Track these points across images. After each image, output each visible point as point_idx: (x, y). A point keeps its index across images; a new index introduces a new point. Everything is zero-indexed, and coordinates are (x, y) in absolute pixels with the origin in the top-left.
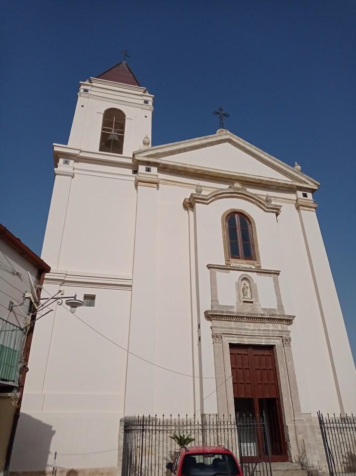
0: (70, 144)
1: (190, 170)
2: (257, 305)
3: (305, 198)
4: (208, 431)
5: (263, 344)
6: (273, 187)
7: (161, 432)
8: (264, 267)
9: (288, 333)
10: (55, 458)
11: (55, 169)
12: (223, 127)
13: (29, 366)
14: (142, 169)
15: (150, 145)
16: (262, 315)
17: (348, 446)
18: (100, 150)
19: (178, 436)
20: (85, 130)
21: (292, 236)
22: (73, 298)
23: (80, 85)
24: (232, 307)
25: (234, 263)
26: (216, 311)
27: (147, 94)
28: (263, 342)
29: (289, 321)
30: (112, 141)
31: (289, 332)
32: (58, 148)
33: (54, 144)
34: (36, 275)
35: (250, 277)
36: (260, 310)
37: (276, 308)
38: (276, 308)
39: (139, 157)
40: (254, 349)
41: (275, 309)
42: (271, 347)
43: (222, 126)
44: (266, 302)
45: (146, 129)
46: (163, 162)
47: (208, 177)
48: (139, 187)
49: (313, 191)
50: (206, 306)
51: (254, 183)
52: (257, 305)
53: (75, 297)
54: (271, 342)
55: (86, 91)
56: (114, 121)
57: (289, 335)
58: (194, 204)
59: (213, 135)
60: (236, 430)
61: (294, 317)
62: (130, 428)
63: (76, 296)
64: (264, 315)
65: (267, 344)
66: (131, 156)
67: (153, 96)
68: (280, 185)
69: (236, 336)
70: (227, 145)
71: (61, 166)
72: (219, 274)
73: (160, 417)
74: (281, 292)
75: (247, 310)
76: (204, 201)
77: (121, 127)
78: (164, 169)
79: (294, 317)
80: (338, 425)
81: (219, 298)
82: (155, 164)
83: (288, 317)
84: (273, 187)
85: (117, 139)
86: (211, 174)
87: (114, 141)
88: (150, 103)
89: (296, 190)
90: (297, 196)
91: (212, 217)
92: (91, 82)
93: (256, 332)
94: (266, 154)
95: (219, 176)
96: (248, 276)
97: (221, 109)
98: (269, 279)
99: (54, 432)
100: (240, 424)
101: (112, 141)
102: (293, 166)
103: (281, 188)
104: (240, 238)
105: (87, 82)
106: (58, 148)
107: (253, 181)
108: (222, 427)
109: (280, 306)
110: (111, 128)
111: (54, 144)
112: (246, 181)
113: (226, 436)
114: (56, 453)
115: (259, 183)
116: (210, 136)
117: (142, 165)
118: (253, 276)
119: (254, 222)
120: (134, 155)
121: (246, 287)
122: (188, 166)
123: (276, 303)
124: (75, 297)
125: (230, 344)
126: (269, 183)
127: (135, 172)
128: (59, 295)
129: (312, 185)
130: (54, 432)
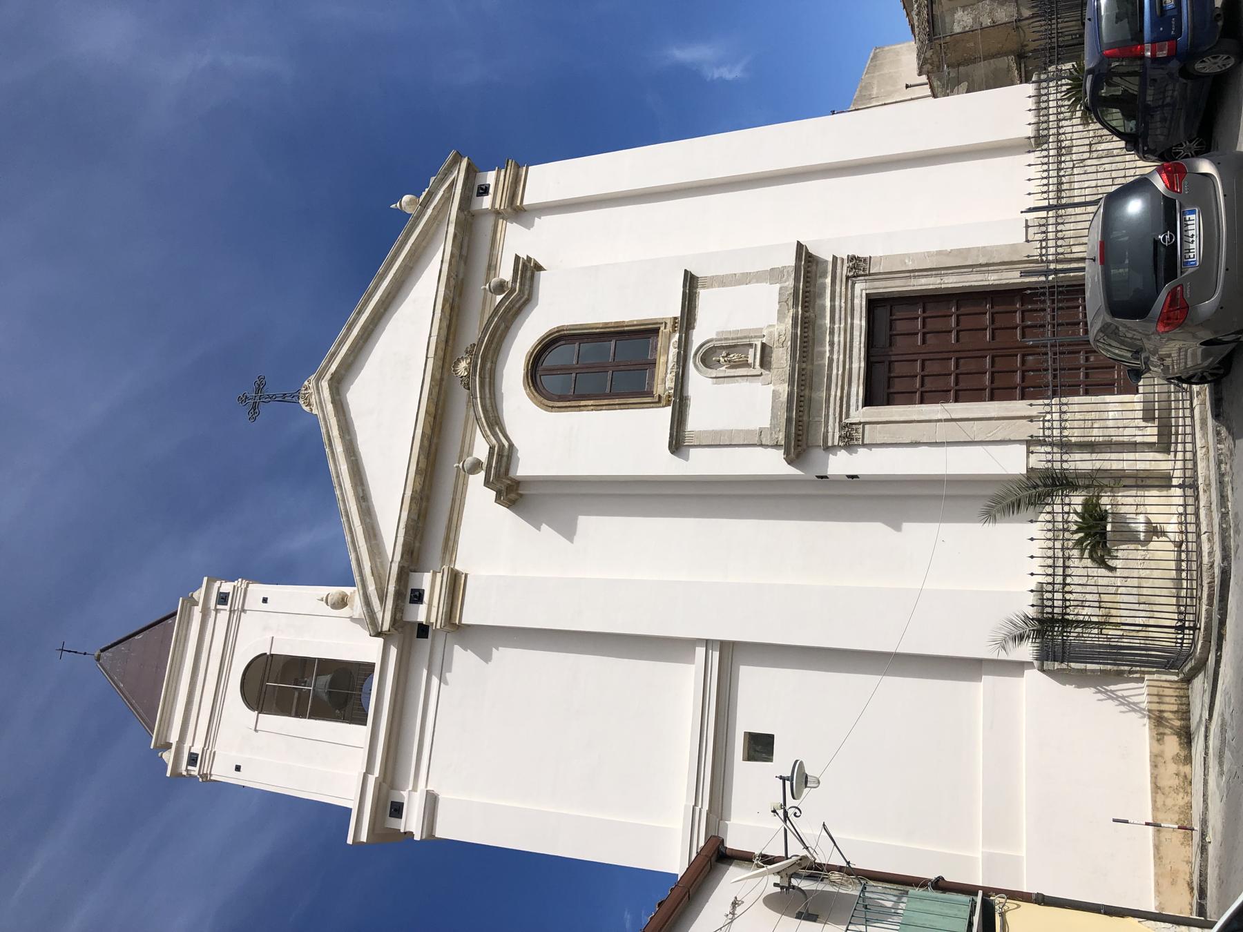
0: (353, 804)
1: (418, 488)
2: (771, 333)
3: (491, 190)
4: (1065, 466)
5: (864, 323)
6: (462, 270)
7: (1069, 571)
8: (675, 310)
10: (1126, 822)
11: (417, 838)
12: (296, 395)
13: (933, 876)
14: (421, 614)
15: (348, 590)
16: (795, 325)
17: (1120, 423)
18: (363, 722)
19: (1077, 536)
20: (320, 763)
21: (601, 235)
22: (788, 783)
23: (176, 774)
24: (775, 394)
25: (664, 381)
26: (787, 436)
27: (199, 595)
28: (860, 323)
29: (807, 262)
30: (326, 690)
31: (835, 258)
32: (360, 831)
33: (350, 841)
34: (724, 866)
35: (701, 346)
36: (782, 327)
37: (778, 286)
38: (778, 286)
39: (385, 619)
42: (874, 303)
43: (291, 398)
44: (760, 312)
45: (309, 597)
46: (398, 558)
47: (435, 440)
48: (464, 622)
49: (471, 173)
50: (773, 463)
51: (450, 321)
52: (771, 333)
53: (783, 779)
54: (860, 303)
55: (193, 759)
56: (282, 685)
58: (513, 480)
59: (322, 423)
60: (1064, 400)
61: (800, 246)
62: (1058, 649)
63: (781, 778)
64: (795, 319)
65: (864, 314)
66: (380, 641)
67: (205, 579)
68: (457, 253)
70: (355, 395)
71: (412, 822)
72: (695, 422)
73: (1033, 583)
74: (738, 271)
75: (782, 358)
76: (504, 457)
77: (298, 667)
78: (413, 558)
79: (800, 246)
80: (1052, 132)
82: (404, 574)
84: (462, 270)
85: (326, 679)
86: (428, 431)
87: (332, 684)
88: (227, 587)
90: (486, 212)
91: (550, 439)
92: (168, 746)
93: (836, 339)
94: (371, 285)
95: (433, 410)
96: (696, 354)
97: (244, 399)
98: (704, 297)
100: (1050, 393)
101: (326, 690)
102: (403, 217)
103: (465, 249)
104: (604, 365)
105: (168, 757)
106: (360, 831)
107: (445, 325)
108: (1056, 432)
109: (774, 275)
110: (296, 694)
111: (350, 841)
112: (447, 342)
113: (1076, 424)
114: (1115, 821)
115: (452, 308)
116: (323, 430)
117: (402, 611)
118: (699, 336)
119: (559, 330)
120: (378, 634)
121: (728, 355)
122: (409, 493)
124: (783, 779)
125: (868, 401)
126: (452, 282)
127: (423, 630)
128: (781, 812)
129: (459, 174)
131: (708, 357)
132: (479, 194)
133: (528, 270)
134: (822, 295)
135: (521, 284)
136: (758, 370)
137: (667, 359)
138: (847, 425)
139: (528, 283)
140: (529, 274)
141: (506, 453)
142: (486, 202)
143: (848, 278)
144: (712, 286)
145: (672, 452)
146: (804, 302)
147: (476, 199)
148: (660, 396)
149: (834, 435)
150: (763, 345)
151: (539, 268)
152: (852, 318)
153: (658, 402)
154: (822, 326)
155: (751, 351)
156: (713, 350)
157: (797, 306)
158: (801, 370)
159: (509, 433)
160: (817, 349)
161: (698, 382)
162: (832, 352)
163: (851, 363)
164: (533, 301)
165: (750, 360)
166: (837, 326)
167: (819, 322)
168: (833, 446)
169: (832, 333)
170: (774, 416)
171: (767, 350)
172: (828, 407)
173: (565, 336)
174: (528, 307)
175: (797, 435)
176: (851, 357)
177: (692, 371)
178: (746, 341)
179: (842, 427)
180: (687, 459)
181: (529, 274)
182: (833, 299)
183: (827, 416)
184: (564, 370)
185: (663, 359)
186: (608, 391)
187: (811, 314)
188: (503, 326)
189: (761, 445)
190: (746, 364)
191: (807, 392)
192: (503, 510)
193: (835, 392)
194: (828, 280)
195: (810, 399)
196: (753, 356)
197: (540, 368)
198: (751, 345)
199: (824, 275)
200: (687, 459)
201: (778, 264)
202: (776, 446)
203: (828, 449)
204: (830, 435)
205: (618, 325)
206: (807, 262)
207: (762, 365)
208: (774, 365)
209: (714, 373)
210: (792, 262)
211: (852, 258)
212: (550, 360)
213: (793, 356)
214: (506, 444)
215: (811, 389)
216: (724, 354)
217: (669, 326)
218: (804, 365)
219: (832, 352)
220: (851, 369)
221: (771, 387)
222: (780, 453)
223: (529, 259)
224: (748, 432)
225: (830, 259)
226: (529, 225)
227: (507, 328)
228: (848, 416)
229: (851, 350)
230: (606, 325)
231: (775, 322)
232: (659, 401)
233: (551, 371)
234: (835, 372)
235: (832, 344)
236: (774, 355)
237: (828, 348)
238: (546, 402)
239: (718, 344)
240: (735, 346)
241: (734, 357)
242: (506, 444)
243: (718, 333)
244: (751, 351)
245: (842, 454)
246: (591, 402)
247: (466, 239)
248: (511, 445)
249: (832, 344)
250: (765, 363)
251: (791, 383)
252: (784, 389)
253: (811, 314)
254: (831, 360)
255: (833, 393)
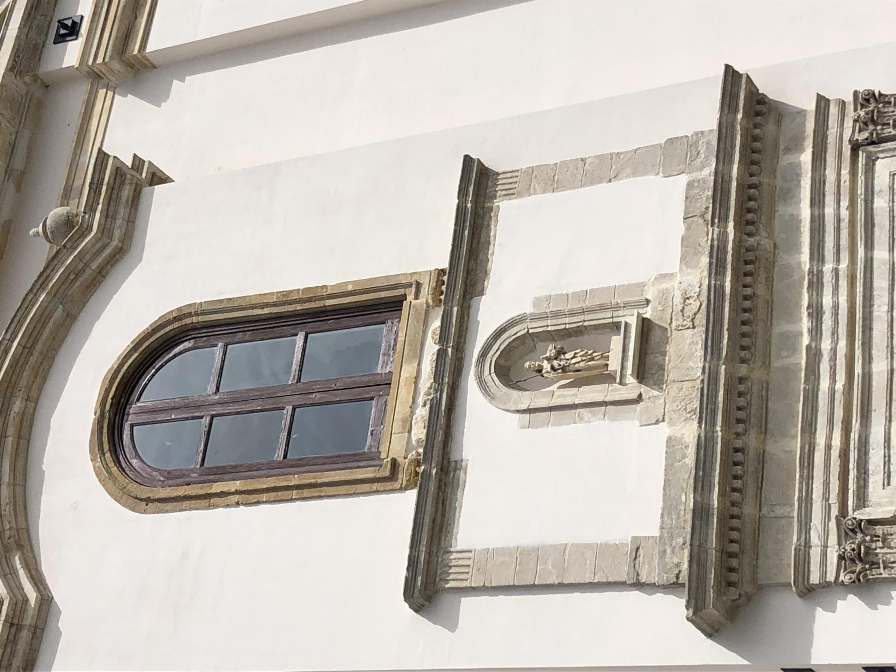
2: (664, 296)
3: (84, 29)
8: (437, 254)
9: (834, 110)
25: (404, 430)
26: (697, 559)
29: (751, 117)
31: (822, 103)
37: (684, 179)
40: (482, 293)
41: (690, 185)
44: (626, 243)
52: (664, 296)
57: (842, 104)
61: (731, 76)
69: (856, 425)
72: (479, 525)
74: (590, 151)
75: (686, 354)
79: (731, 76)
81: (621, 533)
83: (136, 351)
89: (36, 78)
90: (69, 77)
93: (827, 301)
96: (483, 354)
98: (509, 217)
99: (159, 106)
109: (672, 154)
118: (491, 313)
119: (180, 315)
121: (555, 356)
123: (653, 182)
130: (159, 106)
131: (512, 365)
132: (61, 39)
133: (128, 187)
134: (791, 194)
135: (106, 215)
136: (632, 387)
137: (414, 376)
138: (859, 527)
139: (122, 212)
140: (126, 192)
141: (28, 620)
142: (71, 54)
143: (856, 147)
144: (528, 191)
145: (418, 609)
146: (743, 210)
147: (52, 49)
148: (394, 463)
149: (826, 554)
150: (645, 326)
151: (158, 178)
152: (869, 245)
153: (389, 478)
154: (790, 271)
155: (616, 342)
156: (526, 344)
157: (724, 219)
158: (736, 384)
159: (45, 569)
160: (780, 327)
161: (488, 423)
162: (816, 332)
163: (868, 359)
164: (134, 250)
165: (614, 364)
166: (828, 267)
167: (783, 259)
168: (825, 586)
169: (816, 284)
170: (669, 507)
171: (656, 335)
172: (808, 478)
173: (194, 328)
174: (120, 267)
175: (726, 555)
176: (867, 345)
177: (473, 396)
178: (605, 317)
179: (850, 530)
180: (452, 626)
181: (126, 192)
182: (817, 200)
183: (807, 501)
184: (189, 409)
185: (408, 371)
186: (279, 455)
187: (761, 240)
188: (59, 313)
189: (638, 585)
190: (605, 377)
191: (752, 440)
192: (709, 641)
193: (827, 438)
194: (806, 157)
195: (762, 458)
196: (618, 352)
197: (133, 408)
198: (616, 327)
199: (796, 145)
200: (452, 626)
201: (686, 130)
202: (673, 587)
203: (809, 592)
204: (815, 554)
205: (312, 294)
206: (751, 117)
207: (641, 374)
208: (672, 374)
209: (526, 399)
210: (708, 117)
211: (867, 99)
212: (157, 389)
213: (712, 346)
214: (32, 595)
215: (764, 430)
216: (551, 351)
217: (425, 291)
218: (743, 370)
219: (816, 332)
220: (867, 377)
221: (664, 431)
222: (676, 606)
223: (138, 162)
224: (603, 550)
225: (810, 106)
226: (157, 98)
227: (70, 319)
228: (862, 500)
229: (868, 328)
230: (285, 298)
231: (676, 269)
232: (393, 475)
233: (157, 415)
234: (824, 384)
235: (816, 313)
236: (671, 349)
237: (805, 324)
238: (133, 487)
239: (536, 327)
240: (579, 331)
241: (574, 357)
242: (32, 595)
243: (537, 302)
244: (616, 342)
245: (850, 606)
246: (237, 485)
247: (26, 134)
248: (46, 601)
249: (816, 313)
250: (648, 364)
251: (706, 414)
252: (689, 432)
253: (761, 240)
254: (814, 355)
255: (821, 440)
